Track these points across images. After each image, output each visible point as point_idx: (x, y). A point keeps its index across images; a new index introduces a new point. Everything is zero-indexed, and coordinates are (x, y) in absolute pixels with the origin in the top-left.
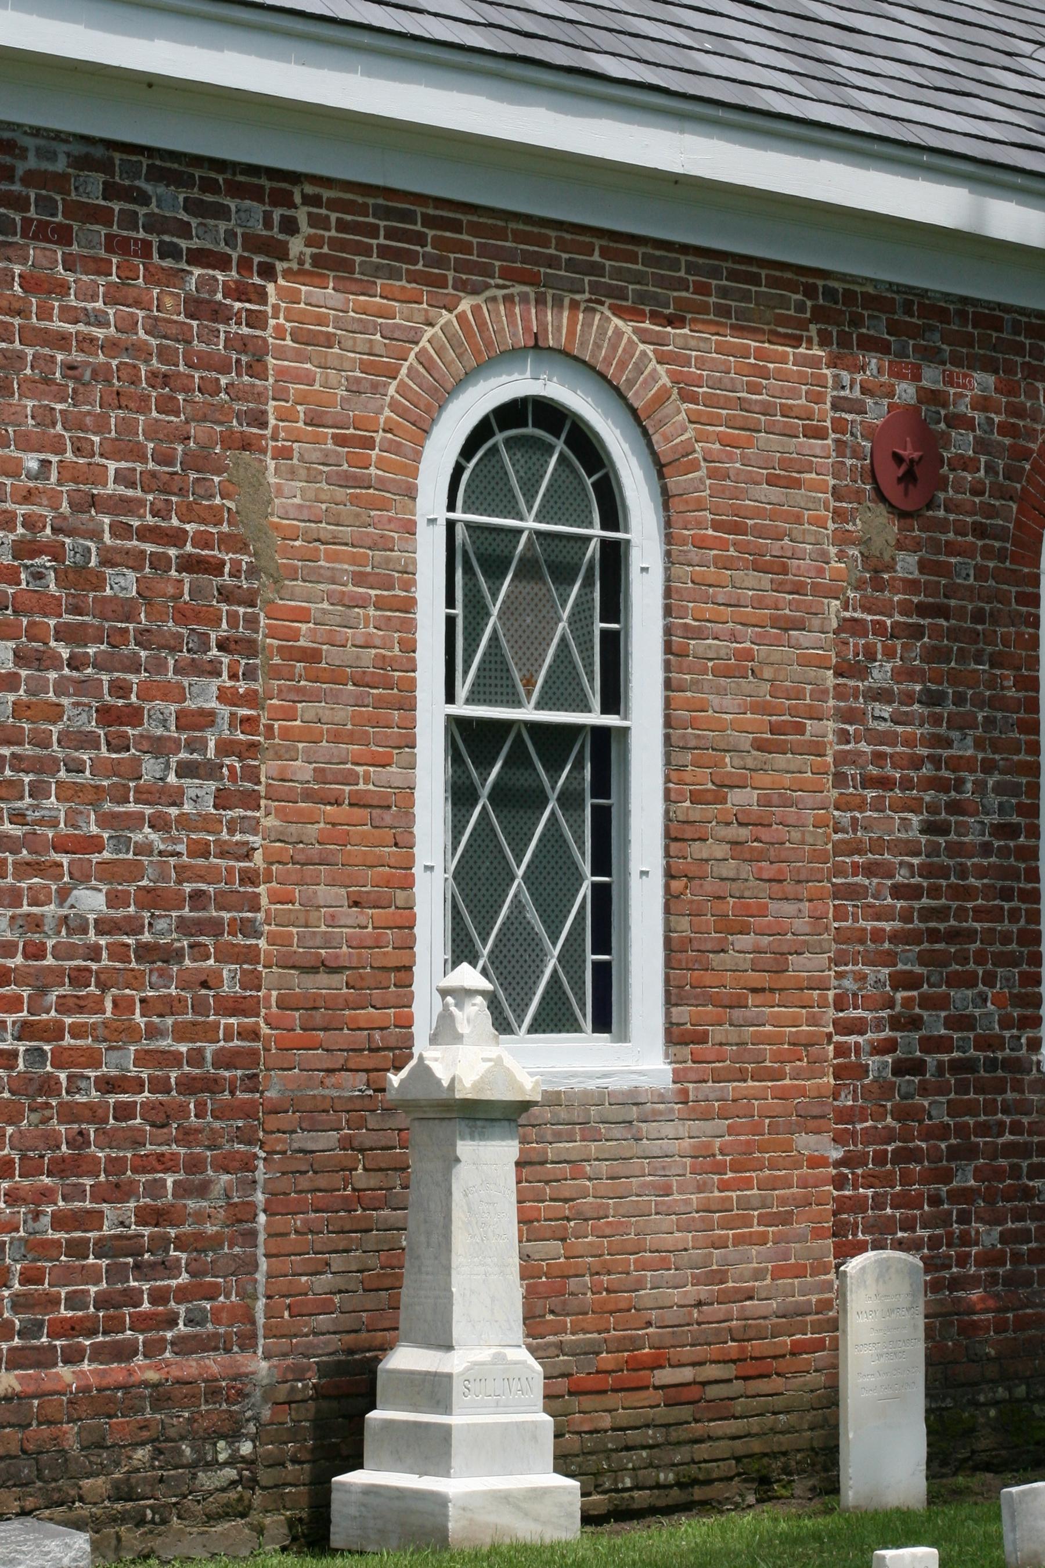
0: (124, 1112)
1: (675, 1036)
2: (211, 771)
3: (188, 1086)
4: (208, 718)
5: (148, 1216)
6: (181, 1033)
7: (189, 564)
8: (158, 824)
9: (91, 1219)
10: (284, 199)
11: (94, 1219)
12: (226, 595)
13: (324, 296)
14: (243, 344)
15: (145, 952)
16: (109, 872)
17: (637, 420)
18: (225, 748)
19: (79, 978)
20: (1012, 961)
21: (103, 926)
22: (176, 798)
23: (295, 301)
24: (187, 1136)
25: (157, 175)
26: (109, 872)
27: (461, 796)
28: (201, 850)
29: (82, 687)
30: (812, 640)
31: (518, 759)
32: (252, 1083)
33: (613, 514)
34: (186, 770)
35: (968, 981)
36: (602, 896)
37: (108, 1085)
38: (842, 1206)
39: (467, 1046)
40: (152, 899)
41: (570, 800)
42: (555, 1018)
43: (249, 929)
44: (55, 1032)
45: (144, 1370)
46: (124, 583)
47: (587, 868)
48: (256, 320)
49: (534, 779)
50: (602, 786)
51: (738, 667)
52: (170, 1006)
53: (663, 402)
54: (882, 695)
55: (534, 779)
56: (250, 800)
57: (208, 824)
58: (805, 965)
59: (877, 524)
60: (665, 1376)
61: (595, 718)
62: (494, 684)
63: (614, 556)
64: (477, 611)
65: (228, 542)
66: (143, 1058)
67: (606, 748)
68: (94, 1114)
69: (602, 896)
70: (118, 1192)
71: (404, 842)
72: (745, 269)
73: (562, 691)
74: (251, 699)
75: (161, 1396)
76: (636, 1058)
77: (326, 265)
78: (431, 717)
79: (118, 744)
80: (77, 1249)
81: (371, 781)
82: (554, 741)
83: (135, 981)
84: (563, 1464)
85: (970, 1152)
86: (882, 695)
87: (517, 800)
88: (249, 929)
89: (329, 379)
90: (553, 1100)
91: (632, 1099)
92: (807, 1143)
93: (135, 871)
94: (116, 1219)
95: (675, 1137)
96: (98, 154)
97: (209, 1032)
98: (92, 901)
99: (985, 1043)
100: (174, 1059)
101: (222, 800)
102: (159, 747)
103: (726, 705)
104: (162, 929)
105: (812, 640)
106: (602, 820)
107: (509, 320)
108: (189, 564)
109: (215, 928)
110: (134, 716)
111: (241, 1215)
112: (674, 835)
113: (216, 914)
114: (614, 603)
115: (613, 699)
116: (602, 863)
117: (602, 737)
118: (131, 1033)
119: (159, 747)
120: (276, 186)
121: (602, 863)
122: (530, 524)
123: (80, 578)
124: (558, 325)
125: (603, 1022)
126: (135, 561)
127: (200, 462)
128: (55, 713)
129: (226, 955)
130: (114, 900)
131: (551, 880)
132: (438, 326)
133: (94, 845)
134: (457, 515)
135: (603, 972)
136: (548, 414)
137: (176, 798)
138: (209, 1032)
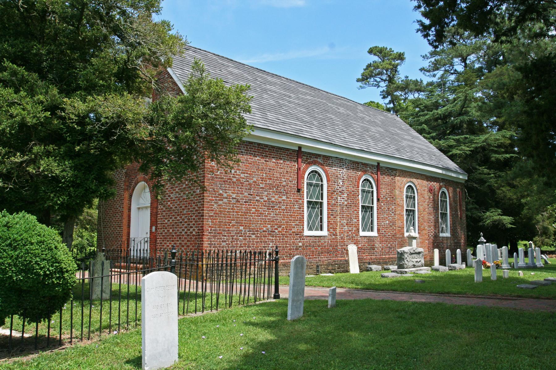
13: (399, 178)
16: (389, 220)
17: (416, 186)
23: (397, 178)
27: (308, 207)
31: (313, 204)
33: (322, 181)
36: (321, 218)
41: (318, 208)
42: (368, 231)
45: (391, 256)
49: (410, 212)
50: (321, 207)
51: (422, 205)
53: (421, 185)
55: (410, 212)
59: (429, 194)
64: (310, 191)
67: (321, 204)
69: (321, 218)
72: (422, 175)
73: (411, 207)
75: (392, 258)
76: (375, 234)
77: (399, 176)
82: (316, 203)
87: (366, 212)
94: (389, 245)
96: (387, 168)
103: (421, 208)
104: (391, 224)
106: (321, 211)
107: (409, 180)
114: (322, 190)
115: (322, 199)
120: (396, 170)
121: (321, 214)
123: (386, 199)
124: (411, 180)
125: (321, 230)
127: (392, 190)
132: (405, 180)
135: (321, 225)
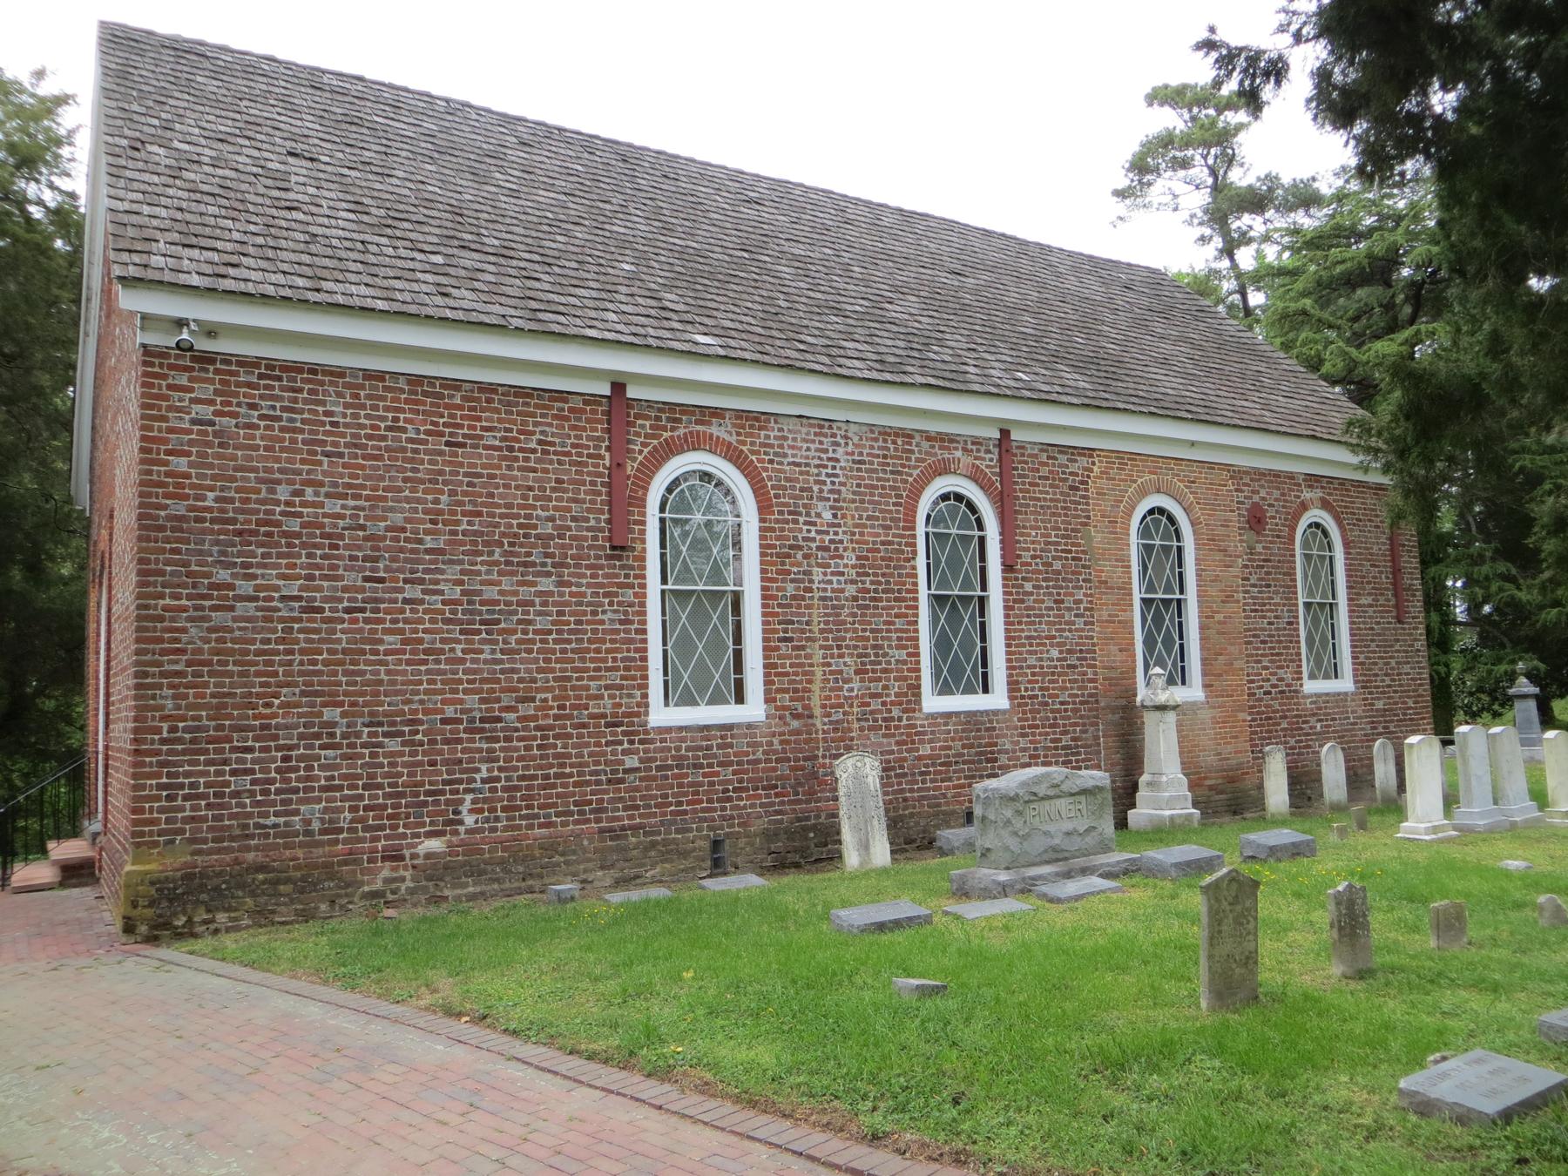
0: (1066, 710)
1: (1206, 686)
2: (1082, 616)
3: (1082, 703)
4: (1080, 601)
5: (1073, 739)
6: (1079, 688)
7: (1074, 559)
8: (1070, 631)
9: (1059, 740)
10: (1091, 456)
11: (1059, 740)
12: (1084, 567)
14: (1084, 497)
15: (1069, 666)
18: (1086, 609)
19: (1053, 674)
20: (1292, 661)
21: (1059, 660)
22: (1073, 623)
24: (1081, 717)
25: (1061, 452)
26: (1059, 645)
27: (935, 620)
28: (1081, 637)
29: (1050, 594)
30: (1235, 571)
32: (1097, 702)
33: (980, 525)
34: (1076, 616)
35: (1281, 667)
36: (1182, 646)
37: (1062, 703)
38: (1253, 733)
39: (1149, 689)
40: (1070, 652)
43: (1094, 659)
44: (1047, 689)
46: (1057, 565)
47: (730, 644)
48: (1086, 490)
52: (1075, 681)
54: (1254, 586)
55: (1163, 613)
56: (1092, 623)
57: (1082, 630)
58: (1238, 664)
60: (1208, 782)
61: (979, 593)
62: (943, 583)
63: (982, 540)
65: (1084, 552)
66: (1070, 696)
68: (1059, 711)
70: (1065, 733)
71: (1132, 633)
73: (1169, 589)
74: (1091, 595)
78: (923, 593)
79: (1059, 609)
80: (1056, 748)
81: (1122, 616)
83: (1066, 674)
84: (1195, 805)
85: (1285, 717)
86: (1254, 586)
88: (1094, 659)
89: (1106, 505)
90: (1186, 703)
91: (1194, 704)
92: (1242, 716)
93: (1065, 644)
95: (1206, 715)
97: (1086, 688)
98: (1055, 653)
99: (1288, 685)
100: (1077, 696)
101: (1086, 623)
102: (1069, 609)
103: (1213, 592)
105: (1235, 571)
108: (1074, 559)
109: (1085, 659)
110: (1062, 602)
111: (1096, 738)
112: (1202, 628)
113: (1084, 654)
115: (984, 587)
116: (1181, 638)
117: (1179, 601)
118: (1066, 689)
119: (1069, 609)
122: (1158, 542)
126: (1060, 558)
128: (1043, 601)
129: (1089, 666)
130: (1061, 652)
131: (1168, 643)
133: (1054, 637)
134: (666, 515)
136: (1161, 511)
137: (1073, 623)
138: (1086, 688)
